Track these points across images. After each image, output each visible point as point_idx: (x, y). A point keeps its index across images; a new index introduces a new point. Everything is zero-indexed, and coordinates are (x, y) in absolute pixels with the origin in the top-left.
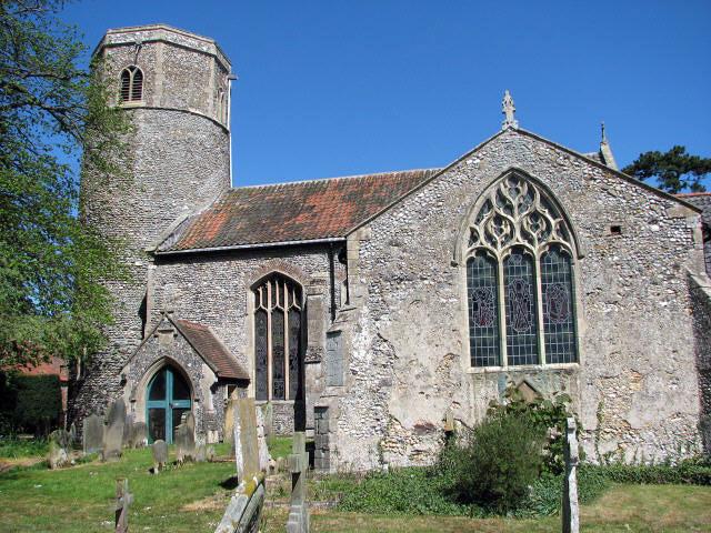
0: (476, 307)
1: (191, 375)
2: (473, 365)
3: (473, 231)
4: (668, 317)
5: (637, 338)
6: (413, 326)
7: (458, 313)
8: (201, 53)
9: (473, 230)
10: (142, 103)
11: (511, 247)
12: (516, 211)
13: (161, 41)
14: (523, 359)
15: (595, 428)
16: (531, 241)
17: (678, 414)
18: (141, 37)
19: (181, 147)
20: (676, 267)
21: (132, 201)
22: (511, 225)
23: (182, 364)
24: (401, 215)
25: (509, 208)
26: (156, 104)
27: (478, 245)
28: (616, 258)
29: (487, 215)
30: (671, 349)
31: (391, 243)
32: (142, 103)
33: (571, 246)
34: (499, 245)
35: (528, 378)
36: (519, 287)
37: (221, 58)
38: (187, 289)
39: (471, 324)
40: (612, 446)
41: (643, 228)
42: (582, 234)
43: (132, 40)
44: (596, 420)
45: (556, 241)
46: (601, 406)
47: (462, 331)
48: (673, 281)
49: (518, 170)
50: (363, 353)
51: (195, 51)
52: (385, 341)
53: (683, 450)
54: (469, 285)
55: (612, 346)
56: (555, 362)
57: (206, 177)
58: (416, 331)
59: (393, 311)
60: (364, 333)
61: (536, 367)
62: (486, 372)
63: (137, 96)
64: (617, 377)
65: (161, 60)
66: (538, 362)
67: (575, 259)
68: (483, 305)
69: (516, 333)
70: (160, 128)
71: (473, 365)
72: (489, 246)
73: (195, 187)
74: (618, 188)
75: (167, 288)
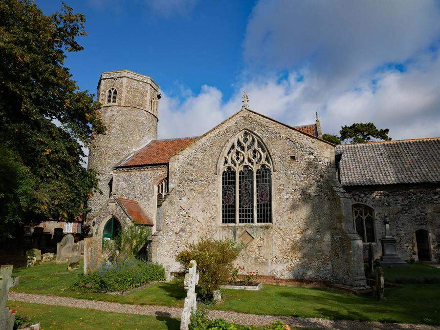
0: (225, 195)
1: (122, 222)
2: (223, 222)
3: (226, 158)
9: (226, 158)
10: (116, 104)
12: (246, 149)
13: (125, 77)
14: (246, 220)
16: (252, 164)
18: (117, 75)
21: (110, 146)
22: (243, 156)
23: (118, 218)
25: (243, 148)
26: (122, 104)
27: (261, 163)
33: (271, 166)
35: (248, 231)
37: (153, 85)
39: (223, 203)
41: (306, 157)
42: (276, 160)
43: (113, 76)
45: (264, 163)
47: (218, 206)
49: (247, 130)
51: (141, 81)
54: (223, 184)
61: (252, 224)
62: (228, 226)
63: (114, 101)
66: (253, 221)
67: (272, 172)
69: (243, 207)
70: (123, 115)
72: (250, 164)
75: (122, 182)
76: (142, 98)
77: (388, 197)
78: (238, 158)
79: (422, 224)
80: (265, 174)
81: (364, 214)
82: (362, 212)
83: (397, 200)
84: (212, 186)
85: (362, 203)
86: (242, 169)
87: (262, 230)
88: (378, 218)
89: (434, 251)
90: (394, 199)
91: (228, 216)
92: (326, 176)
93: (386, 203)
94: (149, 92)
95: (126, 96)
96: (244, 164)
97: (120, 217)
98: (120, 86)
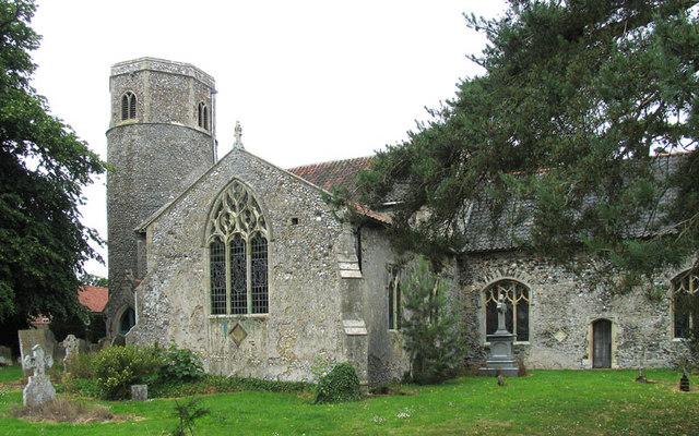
10: (136, 121)
16: (245, 230)
17: (323, 350)
20: (330, 247)
50: (153, 304)
57: (187, 173)
63: (133, 116)
65: (147, 85)
78: (228, 223)
79: (605, 310)
80: (259, 245)
81: (514, 296)
85: (511, 278)
86: (213, 240)
94: (192, 92)
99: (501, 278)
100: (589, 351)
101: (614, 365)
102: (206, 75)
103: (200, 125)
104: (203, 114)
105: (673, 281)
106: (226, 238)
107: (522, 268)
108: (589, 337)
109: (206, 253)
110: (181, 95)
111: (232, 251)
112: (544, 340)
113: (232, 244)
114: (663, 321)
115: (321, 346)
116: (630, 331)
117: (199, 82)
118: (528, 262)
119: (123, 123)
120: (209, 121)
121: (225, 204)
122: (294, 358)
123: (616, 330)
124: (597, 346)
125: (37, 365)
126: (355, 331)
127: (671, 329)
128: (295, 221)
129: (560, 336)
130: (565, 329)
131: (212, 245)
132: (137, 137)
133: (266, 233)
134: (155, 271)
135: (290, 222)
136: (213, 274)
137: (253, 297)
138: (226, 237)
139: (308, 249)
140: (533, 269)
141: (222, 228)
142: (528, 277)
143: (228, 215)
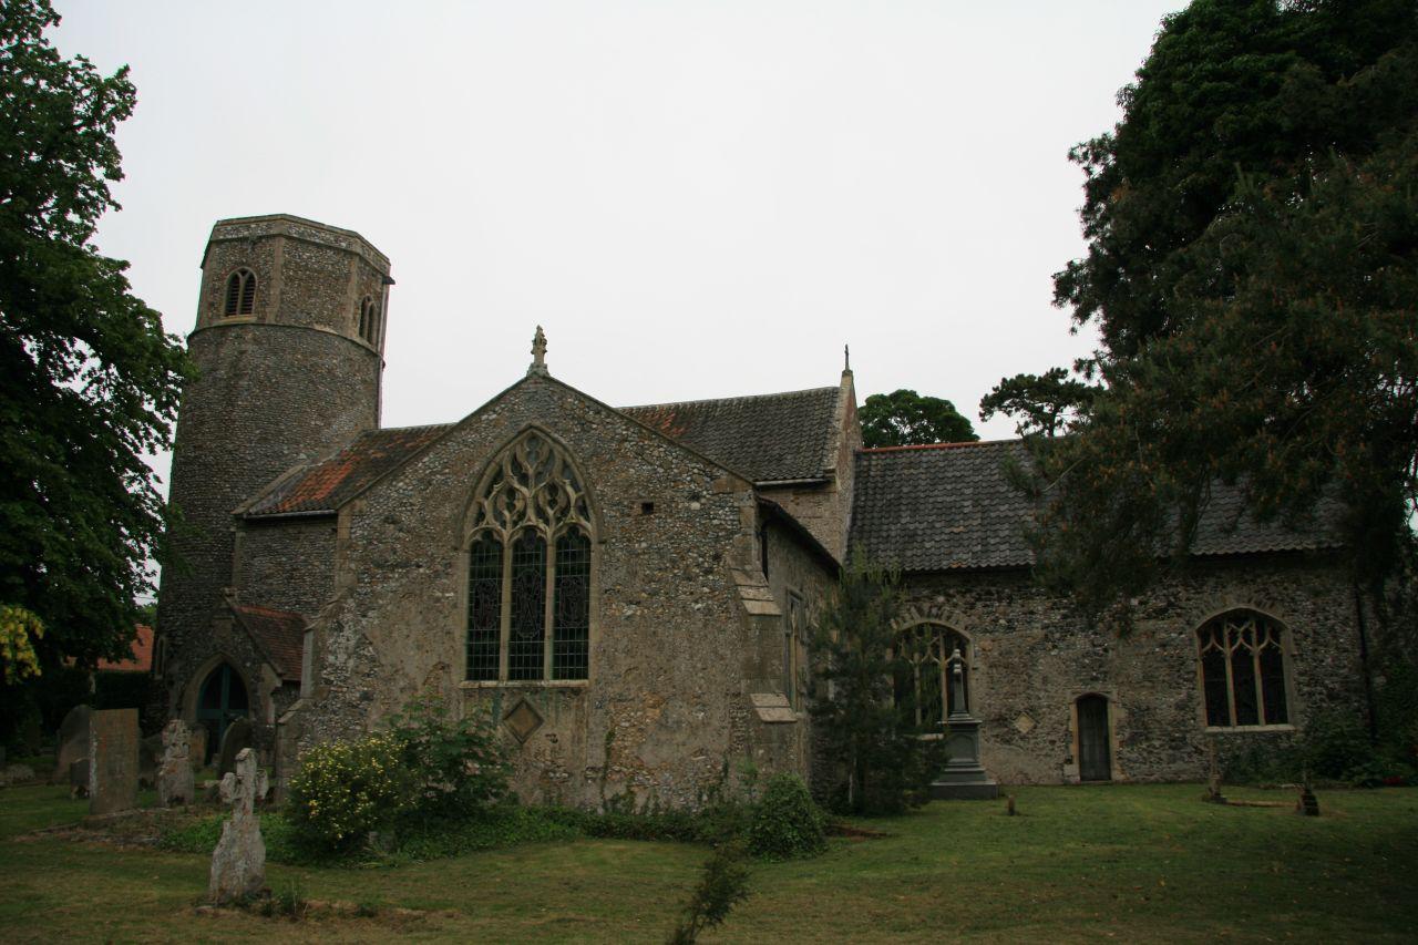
0: (477, 603)
3: (481, 506)
4: (700, 625)
5: (661, 649)
6: (403, 627)
7: (454, 611)
8: (338, 250)
10: (252, 318)
11: (522, 528)
13: (280, 235)
14: (527, 671)
15: (601, 765)
16: (547, 522)
17: (701, 751)
19: (300, 376)
20: (717, 557)
22: (524, 499)
24: (401, 484)
26: (270, 319)
27: (483, 525)
28: (644, 545)
29: (497, 487)
30: (699, 665)
31: (386, 520)
32: (252, 318)
34: (509, 525)
35: (528, 697)
36: (529, 579)
38: (280, 564)
40: (622, 790)
44: (604, 756)
46: (611, 735)
48: (711, 577)
49: (536, 428)
50: (342, 657)
51: (330, 248)
52: (371, 643)
53: (705, 798)
55: (629, 661)
56: (564, 677)
58: (405, 632)
59: (381, 606)
60: (347, 632)
62: (480, 688)
64: (633, 699)
66: (541, 678)
68: (486, 601)
69: (520, 639)
71: (469, 677)
73: (318, 430)
74: (656, 453)
76: (333, 299)
77: (1009, 604)
78: (511, 507)
79: (1095, 679)
80: (574, 548)
81: (942, 653)
82: (938, 647)
83: (1032, 613)
84: (445, 581)
85: (937, 621)
87: (562, 698)
88: (978, 665)
89: (1119, 753)
90: (1025, 609)
91: (481, 664)
92: (335, 633)
93: (1002, 621)
94: (355, 278)
95: (282, 293)
96: (524, 523)
97: (244, 662)
98: (266, 263)
99: (919, 621)
100: (1074, 749)
101: (1117, 775)
102: (378, 253)
103: (361, 334)
104: (367, 318)
105: (1198, 631)
106: (507, 535)
107: (955, 605)
108: (1073, 726)
109: (463, 561)
110: (337, 281)
111: (516, 559)
112: (995, 732)
113: (517, 545)
114: (1190, 697)
115: (696, 743)
116: (1140, 718)
117: (367, 263)
118: (963, 594)
119: (224, 321)
120: (375, 328)
121: (508, 470)
122: (641, 767)
123: (1116, 714)
124: (1086, 743)
125: (243, 795)
126: (775, 715)
127: (1201, 711)
128: (648, 508)
129: (1023, 724)
130: (1032, 712)
131: (475, 547)
132: (250, 348)
133: (589, 527)
134: (351, 591)
135: (637, 509)
136: (475, 603)
137: (557, 649)
138: (506, 533)
139: (673, 561)
140: (972, 606)
141: (498, 516)
142: (965, 620)
143: (511, 492)
